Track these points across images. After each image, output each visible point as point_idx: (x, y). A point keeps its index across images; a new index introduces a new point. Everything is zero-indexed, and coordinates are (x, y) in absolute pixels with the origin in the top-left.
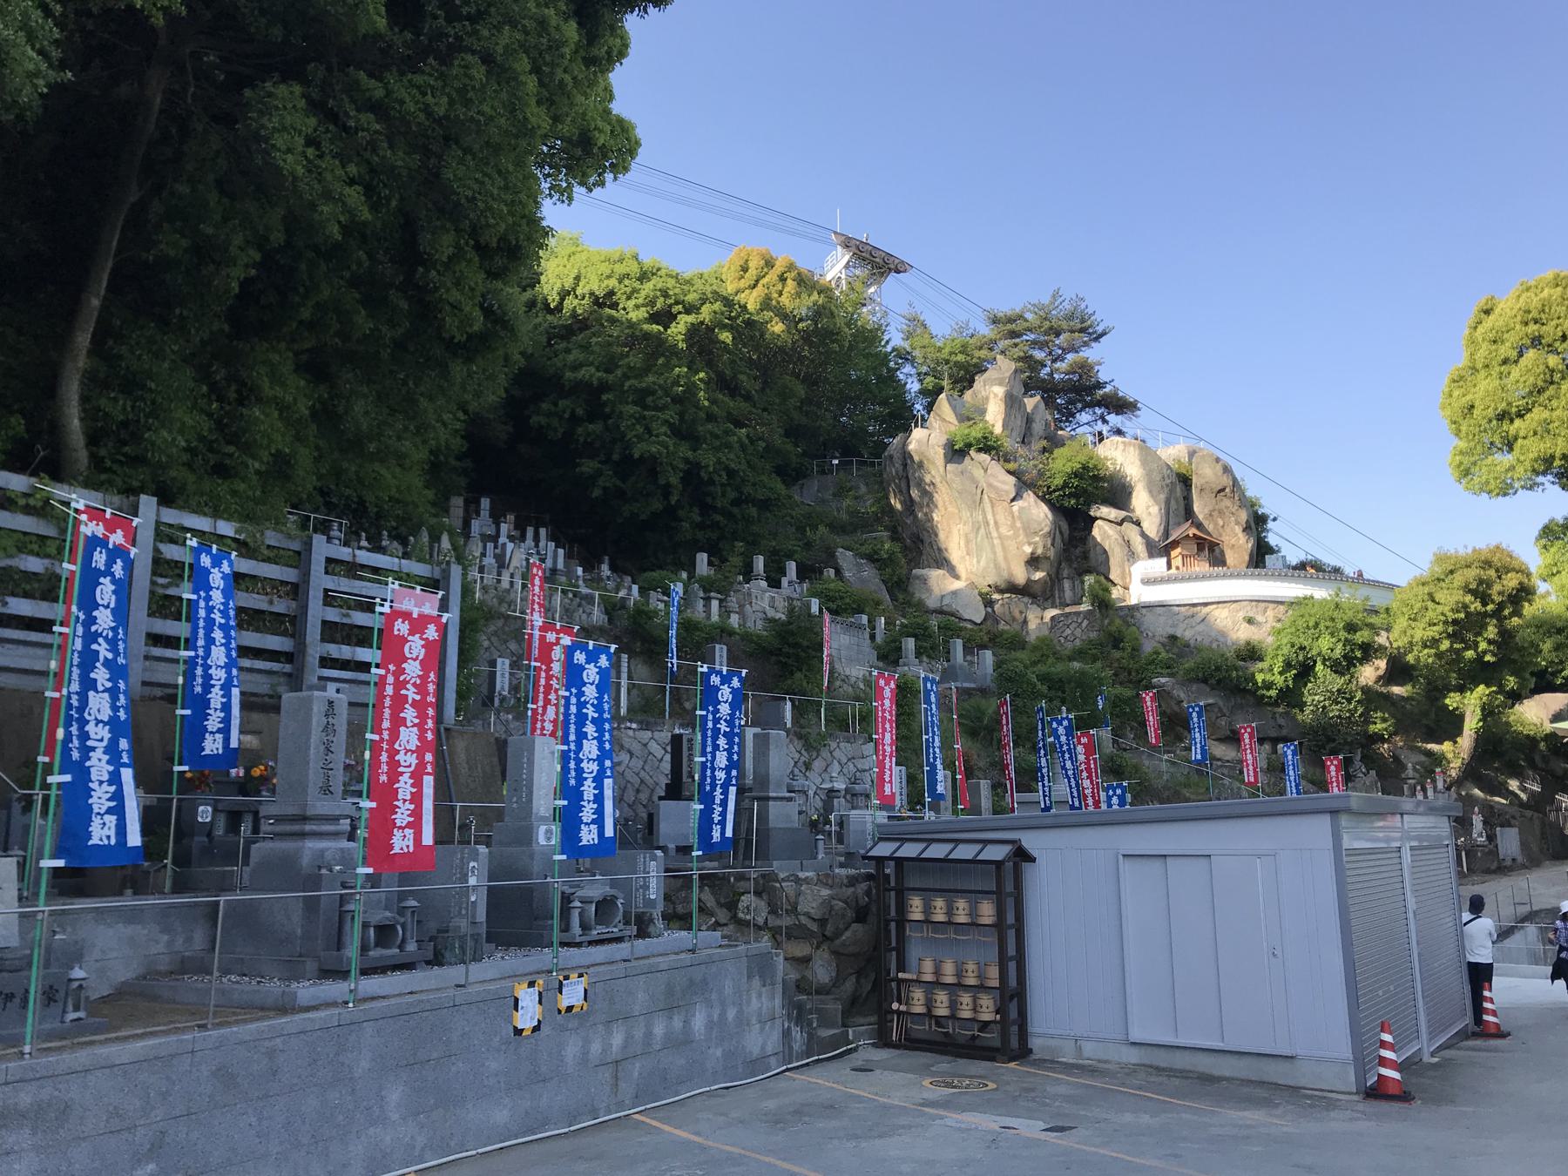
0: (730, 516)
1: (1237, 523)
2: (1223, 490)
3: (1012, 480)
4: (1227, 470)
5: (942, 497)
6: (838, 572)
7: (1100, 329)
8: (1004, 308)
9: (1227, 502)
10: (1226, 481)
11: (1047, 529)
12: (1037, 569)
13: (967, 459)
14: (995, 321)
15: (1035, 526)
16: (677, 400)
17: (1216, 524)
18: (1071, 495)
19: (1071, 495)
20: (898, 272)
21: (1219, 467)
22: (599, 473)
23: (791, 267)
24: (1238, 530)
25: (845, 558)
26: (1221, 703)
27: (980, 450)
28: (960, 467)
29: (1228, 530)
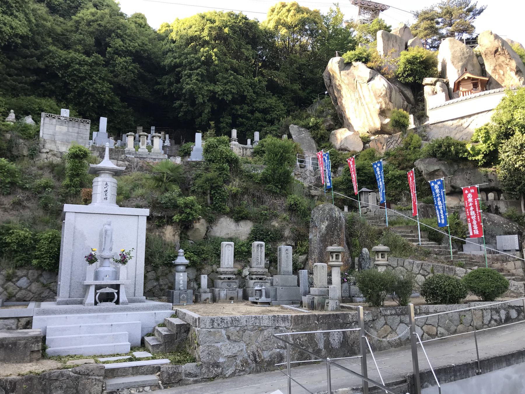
0: (248, 119)
1: (511, 70)
2: (496, 51)
3: (369, 70)
4: (496, 37)
5: (345, 91)
6: (290, 136)
7: (478, 7)
8: (420, 8)
9: (502, 58)
10: (497, 44)
11: (384, 93)
12: (386, 117)
13: (352, 68)
14: (417, 15)
15: (378, 92)
16: (203, 63)
17: (499, 74)
18: (409, 75)
19: (409, 75)
20: (383, 10)
21: (492, 37)
22: (181, 106)
23: (293, 5)
24: (513, 74)
25: (293, 129)
26: (443, 168)
27: (357, 60)
28: (347, 72)
29: (507, 76)
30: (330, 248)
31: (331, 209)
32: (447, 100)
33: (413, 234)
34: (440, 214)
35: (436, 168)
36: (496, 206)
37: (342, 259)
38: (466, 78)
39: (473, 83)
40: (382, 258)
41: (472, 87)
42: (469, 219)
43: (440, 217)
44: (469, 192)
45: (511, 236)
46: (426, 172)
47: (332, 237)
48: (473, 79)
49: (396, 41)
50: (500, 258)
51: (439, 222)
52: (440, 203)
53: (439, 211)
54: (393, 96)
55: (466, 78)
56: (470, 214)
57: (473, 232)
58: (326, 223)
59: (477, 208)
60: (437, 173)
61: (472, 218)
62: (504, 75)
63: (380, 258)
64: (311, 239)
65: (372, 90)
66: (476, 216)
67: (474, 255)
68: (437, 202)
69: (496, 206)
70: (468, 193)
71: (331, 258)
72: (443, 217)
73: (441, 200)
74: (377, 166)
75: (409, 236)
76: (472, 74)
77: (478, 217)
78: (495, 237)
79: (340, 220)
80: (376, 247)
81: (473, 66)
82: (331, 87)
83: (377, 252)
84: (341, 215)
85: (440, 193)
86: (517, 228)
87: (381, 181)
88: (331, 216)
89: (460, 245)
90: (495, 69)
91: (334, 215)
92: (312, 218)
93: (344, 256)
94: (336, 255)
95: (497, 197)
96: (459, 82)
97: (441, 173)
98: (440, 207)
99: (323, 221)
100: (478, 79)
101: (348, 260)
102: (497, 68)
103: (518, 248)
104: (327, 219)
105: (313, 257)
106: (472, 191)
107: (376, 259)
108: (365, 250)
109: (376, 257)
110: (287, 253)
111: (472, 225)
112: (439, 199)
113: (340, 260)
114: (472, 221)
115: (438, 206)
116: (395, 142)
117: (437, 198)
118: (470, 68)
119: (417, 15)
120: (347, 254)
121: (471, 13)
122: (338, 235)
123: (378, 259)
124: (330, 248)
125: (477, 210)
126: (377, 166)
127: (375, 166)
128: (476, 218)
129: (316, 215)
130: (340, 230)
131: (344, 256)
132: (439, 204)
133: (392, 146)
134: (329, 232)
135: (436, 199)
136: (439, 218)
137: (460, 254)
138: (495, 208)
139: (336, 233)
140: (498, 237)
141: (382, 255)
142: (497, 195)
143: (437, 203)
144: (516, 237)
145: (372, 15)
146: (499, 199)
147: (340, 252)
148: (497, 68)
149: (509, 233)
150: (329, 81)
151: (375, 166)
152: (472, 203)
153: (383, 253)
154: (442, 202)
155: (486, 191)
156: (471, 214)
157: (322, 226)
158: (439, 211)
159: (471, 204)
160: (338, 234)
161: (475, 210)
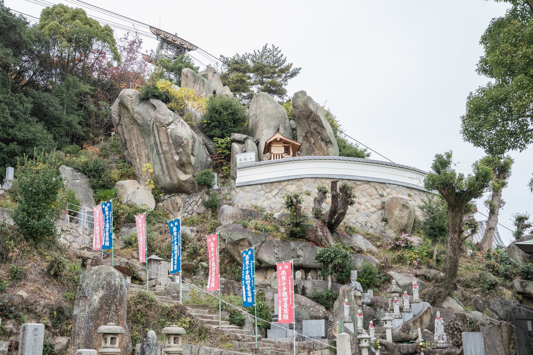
8: (230, 55)
14: (226, 62)
30: (103, 328)
31: (110, 274)
32: (256, 161)
33: (211, 315)
34: (246, 291)
35: (241, 237)
36: (303, 287)
37: (120, 344)
38: (278, 139)
39: (285, 146)
40: (175, 343)
41: (283, 151)
42: (280, 301)
43: (247, 294)
44: (283, 269)
45: (318, 320)
46: (229, 240)
47: (107, 313)
48: (285, 142)
49: (204, 86)
50: (307, 346)
51: (245, 300)
52: (247, 277)
53: (246, 288)
54: (195, 148)
55: (278, 139)
56: (282, 294)
57: (282, 317)
58: (101, 293)
59: (290, 288)
60: (242, 243)
61: (284, 299)
62: (314, 144)
63: (172, 343)
64: (76, 316)
65: (171, 136)
66: (289, 297)
67: (279, 342)
68: (245, 275)
69: (303, 287)
70: (282, 270)
71: (103, 344)
72: (250, 294)
73: (250, 274)
74: (174, 226)
75: (206, 318)
76: (284, 137)
77: (290, 299)
78: (301, 322)
79: (121, 289)
80: (168, 328)
81: (285, 128)
82: (120, 126)
83: (168, 335)
84: (123, 283)
85: (249, 265)
86: (323, 312)
87: (177, 244)
88: (109, 283)
89: (265, 329)
90: (306, 136)
91: (113, 282)
92: (81, 285)
93: (122, 341)
94: (112, 339)
95: (304, 276)
96: (271, 143)
97: (247, 244)
98: (248, 282)
99: (95, 290)
100: (289, 143)
101: (127, 346)
102: (309, 135)
103: (324, 335)
104: (103, 288)
105: (78, 341)
106: (286, 267)
107: (167, 344)
108: (151, 333)
109: (167, 342)
110: (36, 335)
111: (283, 308)
112: (247, 272)
113: (117, 345)
114: (283, 303)
115: (245, 280)
116: (194, 203)
117: (245, 270)
118: (282, 130)
119: (226, 62)
120: (127, 339)
121: (284, 75)
122: (117, 311)
123: (170, 345)
124: (103, 328)
125: (290, 291)
126: (174, 226)
127: (172, 225)
128: (289, 300)
129: (87, 281)
130: (120, 304)
131: (122, 341)
132: (246, 278)
133: (190, 208)
134: (104, 307)
135: (245, 272)
136: (244, 296)
137: (264, 342)
138: (301, 288)
139: (113, 308)
140: (304, 322)
141: (175, 339)
142: (304, 274)
143: (245, 277)
144: (323, 321)
145: (177, 53)
146: (306, 279)
147: (117, 334)
148: (309, 135)
149: (316, 318)
150: (118, 117)
151: (172, 225)
152: (286, 282)
153: (176, 336)
154: (250, 276)
155: (296, 268)
156: (283, 295)
157: (95, 297)
158: (246, 288)
159: (284, 284)
160: (117, 309)
161: (287, 290)
